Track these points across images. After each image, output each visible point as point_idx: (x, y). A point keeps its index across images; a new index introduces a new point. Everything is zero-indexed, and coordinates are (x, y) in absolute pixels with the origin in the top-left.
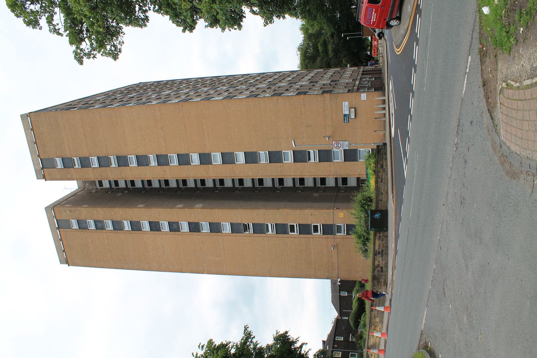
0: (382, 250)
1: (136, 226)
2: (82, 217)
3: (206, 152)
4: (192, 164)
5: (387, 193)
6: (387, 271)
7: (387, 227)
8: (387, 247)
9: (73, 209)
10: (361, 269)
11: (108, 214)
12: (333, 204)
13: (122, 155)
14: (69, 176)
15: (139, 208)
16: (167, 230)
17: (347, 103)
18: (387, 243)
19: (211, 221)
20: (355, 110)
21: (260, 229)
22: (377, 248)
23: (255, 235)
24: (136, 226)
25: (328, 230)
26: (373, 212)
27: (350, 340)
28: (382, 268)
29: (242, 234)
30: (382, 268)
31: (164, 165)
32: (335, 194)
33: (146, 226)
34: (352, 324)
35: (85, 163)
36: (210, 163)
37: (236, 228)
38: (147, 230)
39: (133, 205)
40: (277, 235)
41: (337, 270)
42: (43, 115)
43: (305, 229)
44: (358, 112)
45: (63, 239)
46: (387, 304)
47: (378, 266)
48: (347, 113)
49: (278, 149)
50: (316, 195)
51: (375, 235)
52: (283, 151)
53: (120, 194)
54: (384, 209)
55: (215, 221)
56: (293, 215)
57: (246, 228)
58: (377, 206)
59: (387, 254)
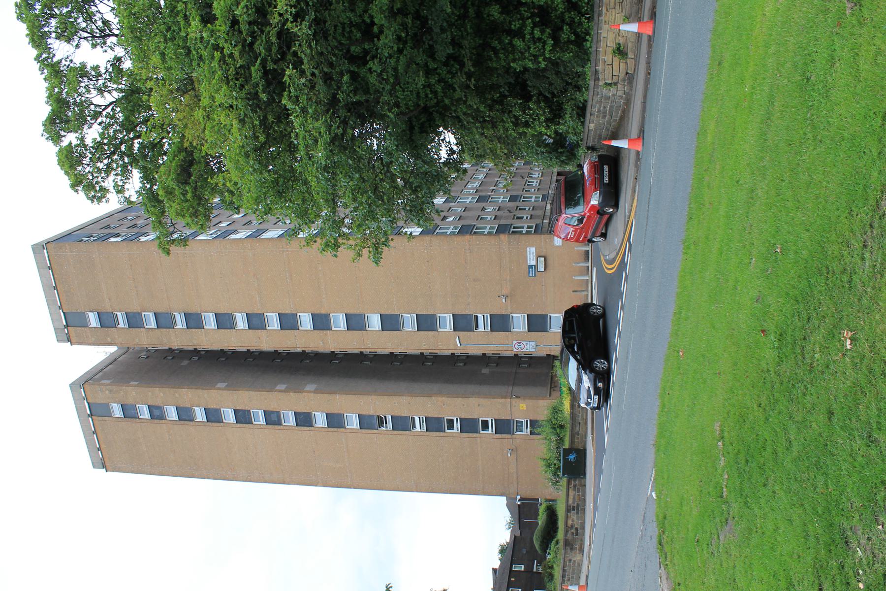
0: (578, 505)
1: (214, 416)
2: (130, 401)
3: (323, 312)
4: (301, 328)
5: (586, 424)
6: (584, 534)
7: (585, 474)
8: (584, 500)
9: (114, 388)
10: (548, 489)
11: (171, 398)
12: (510, 388)
13: (194, 311)
14: (109, 340)
15: (219, 389)
16: (261, 423)
17: (533, 249)
18: (584, 495)
19: (329, 412)
20: (545, 260)
21: (402, 424)
22: (571, 501)
23: (395, 432)
24: (214, 416)
25: (504, 427)
26: (567, 452)
27: (535, 570)
28: (577, 529)
29: (375, 431)
30: (577, 529)
31: (258, 329)
32: (514, 370)
33: (229, 416)
34: (537, 546)
35: (135, 321)
36: (329, 328)
37: (365, 422)
38: (232, 421)
39: (210, 385)
40: (428, 433)
41: (515, 483)
42: (68, 247)
43: (469, 426)
44: (549, 262)
45: (98, 431)
46: (582, 582)
47: (572, 526)
48: (533, 263)
49: (431, 312)
50: (485, 371)
51: (569, 483)
52: (438, 315)
53: (185, 363)
54: (580, 447)
55: (336, 411)
56: (453, 405)
57: (381, 421)
58: (572, 442)
59: (584, 510)
